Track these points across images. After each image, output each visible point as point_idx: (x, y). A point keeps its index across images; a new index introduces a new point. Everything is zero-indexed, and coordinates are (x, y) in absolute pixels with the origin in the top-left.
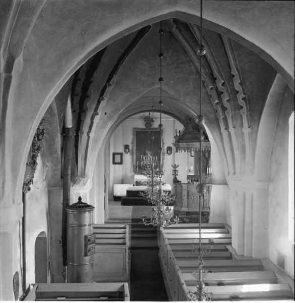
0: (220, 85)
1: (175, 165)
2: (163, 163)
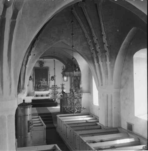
0: (96, 39)
1: (62, 84)
2: (49, 85)
